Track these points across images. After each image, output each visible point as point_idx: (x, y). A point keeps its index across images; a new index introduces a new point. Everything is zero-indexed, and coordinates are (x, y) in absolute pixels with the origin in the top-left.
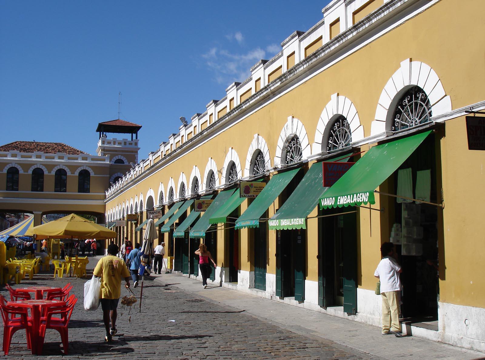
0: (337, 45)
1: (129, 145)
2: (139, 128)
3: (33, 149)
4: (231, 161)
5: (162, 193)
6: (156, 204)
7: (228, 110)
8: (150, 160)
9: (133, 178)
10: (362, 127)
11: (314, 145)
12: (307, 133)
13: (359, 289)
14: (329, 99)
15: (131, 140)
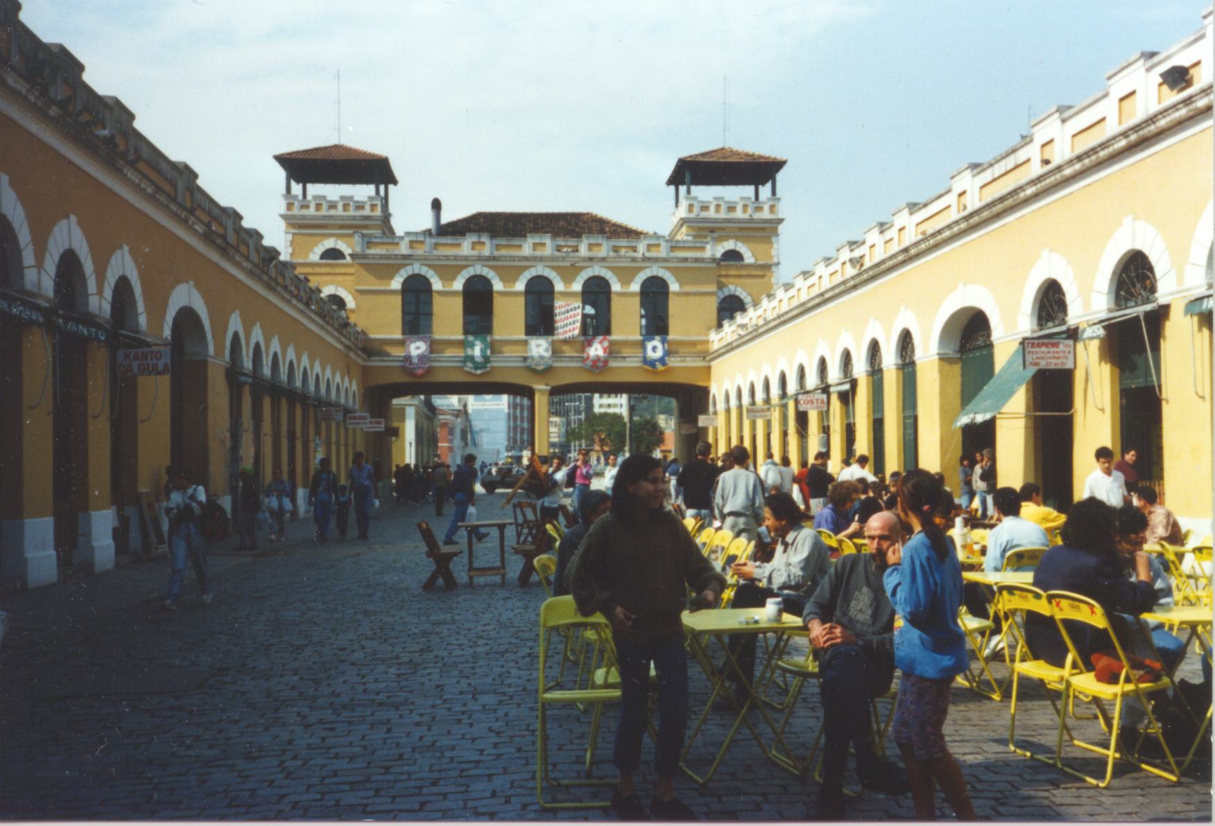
2: (778, 165)
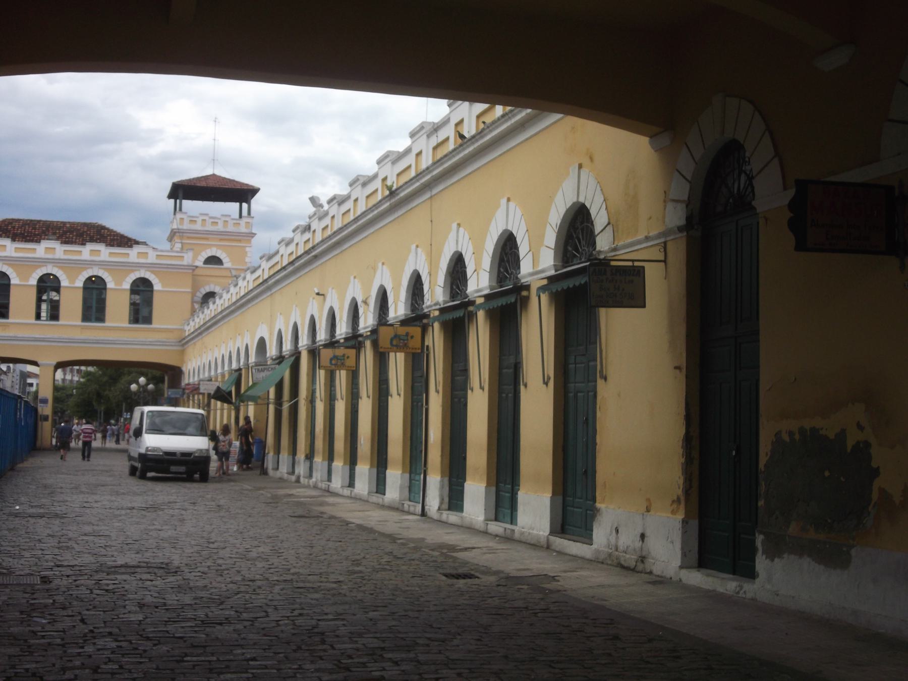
0: (376, 212)
1: (148, 320)
3: (38, 235)
4: (506, 231)
5: (280, 332)
6: (272, 351)
7: (413, 173)
8: (295, 242)
9: (234, 300)
10: (531, 252)
11: (481, 272)
12: (527, 230)
13: (392, 471)
14: (498, 206)
15: (237, 216)
